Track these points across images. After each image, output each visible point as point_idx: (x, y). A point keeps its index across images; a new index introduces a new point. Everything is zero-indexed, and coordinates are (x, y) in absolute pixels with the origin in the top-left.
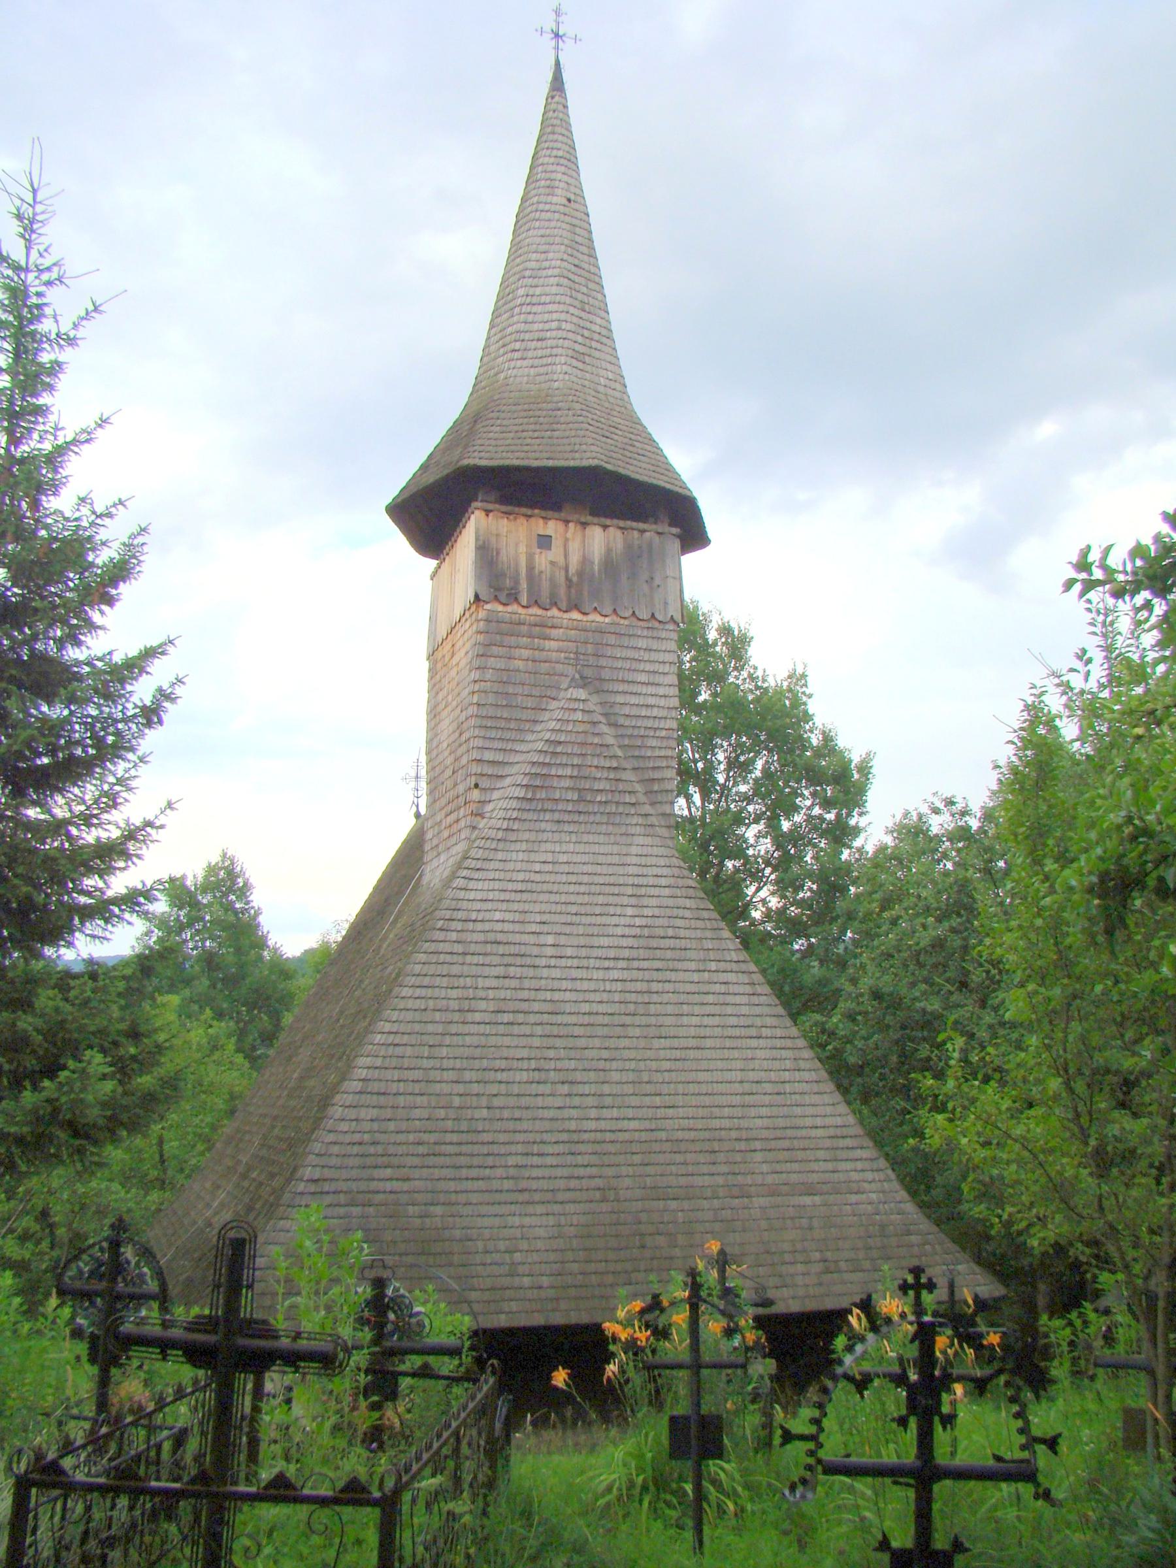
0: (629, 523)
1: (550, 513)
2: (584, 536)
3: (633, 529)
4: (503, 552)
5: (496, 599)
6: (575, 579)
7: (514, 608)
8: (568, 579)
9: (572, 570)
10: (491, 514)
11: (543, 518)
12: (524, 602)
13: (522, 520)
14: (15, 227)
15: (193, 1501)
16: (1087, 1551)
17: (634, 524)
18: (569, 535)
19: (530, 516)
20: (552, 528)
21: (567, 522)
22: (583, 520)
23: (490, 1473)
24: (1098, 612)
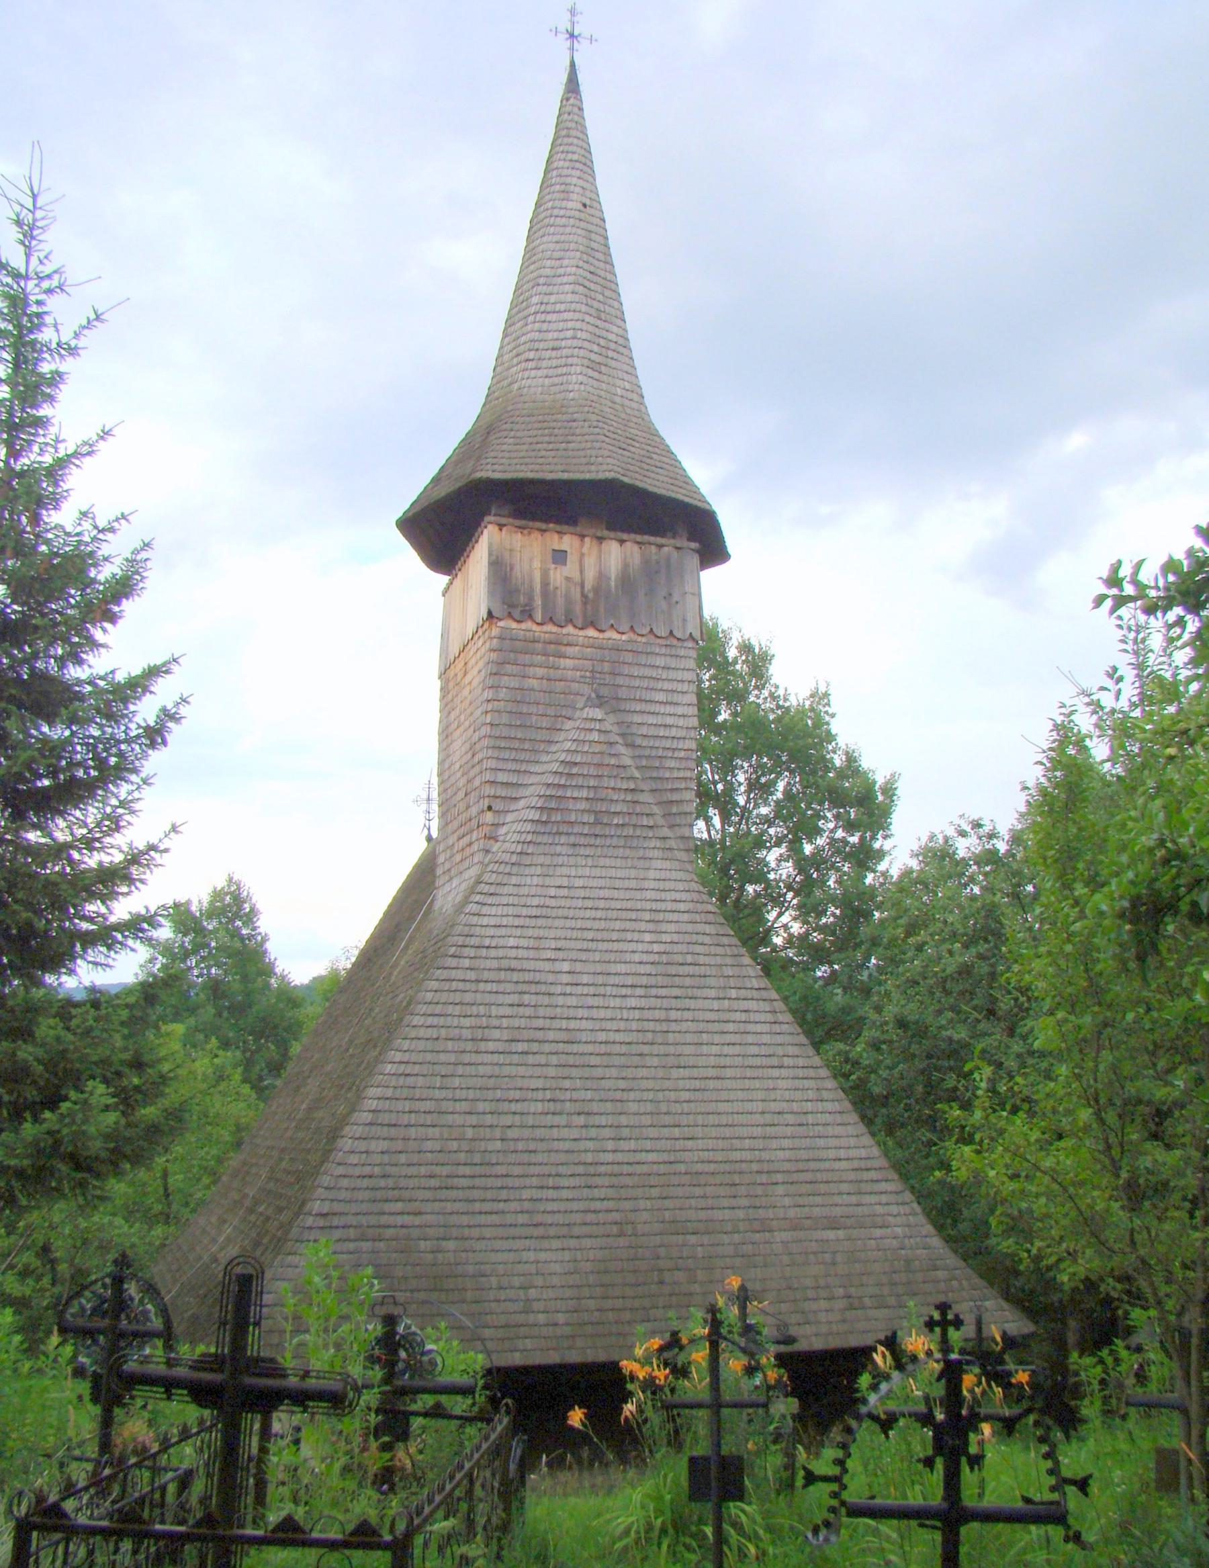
0: (646, 538)
1: (565, 528)
2: (600, 551)
4: (517, 568)
5: (510, 615)
6: (591, 595)
7: (528, 625)
8: (583, 595)
9: (588, 585)
12: (539, 618)
13: (537, 535)
17: (652, 539)
18: (585, 550)
19: (545, 531)
20: (567, 542)
22: (599, 534)
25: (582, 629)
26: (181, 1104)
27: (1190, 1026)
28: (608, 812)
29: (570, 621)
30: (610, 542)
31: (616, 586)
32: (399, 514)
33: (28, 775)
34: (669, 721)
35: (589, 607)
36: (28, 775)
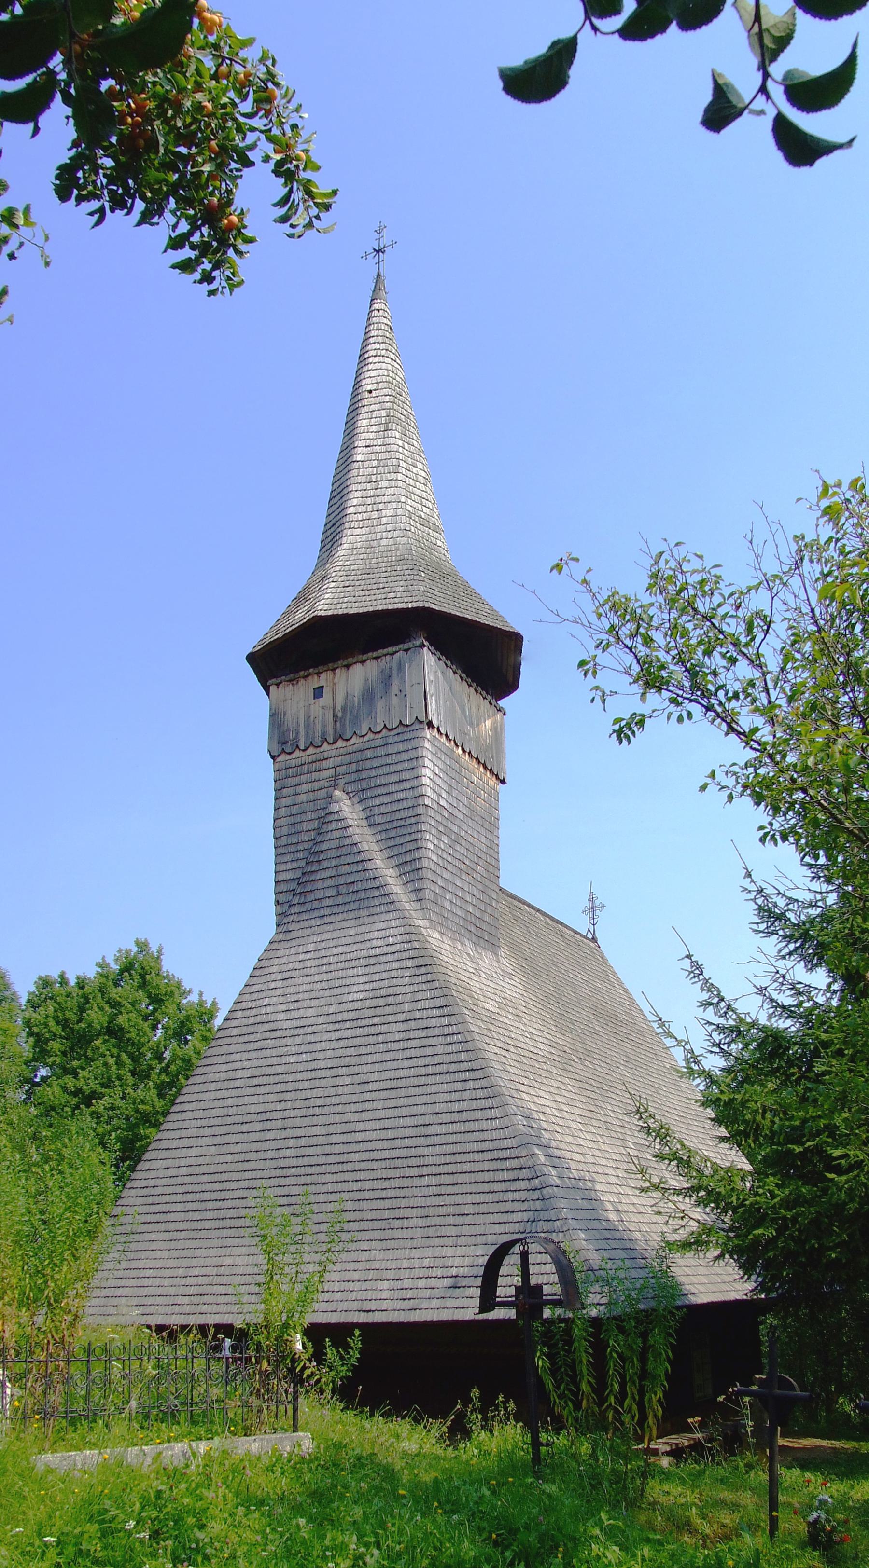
0: (381, 652)
1: (321, 668)
2: (347, 677)
3: (385, 655)
4: (289, 713)
5: (283, 751)
6: (340, 714)
7: (297, 754)
8: (335, 716)
9: (338, 707)
10: (281, 686)
11: (290, 681)
12: (302, 747)
13: (302, 681)
14: (718, 574)
15: (776, 674)
16: (342, 1466)
17: (385, 651)
18: (336, 680)
19: (307, 676)
20: (324, 679)
21: (334, 670)
22: (345, 663)
23: (800, 670)
24: (21, 1246)
25: (334, 743)
26: (699, 1205)
27: (46, 1030)
28: (682, 696)
29: (324, 740)
30: (354, 666)
31: (359, 700)
32: (250, 650)
33: (183, 150)
34: (401, 796)
35: (338, 724)
36: (183, 150)
